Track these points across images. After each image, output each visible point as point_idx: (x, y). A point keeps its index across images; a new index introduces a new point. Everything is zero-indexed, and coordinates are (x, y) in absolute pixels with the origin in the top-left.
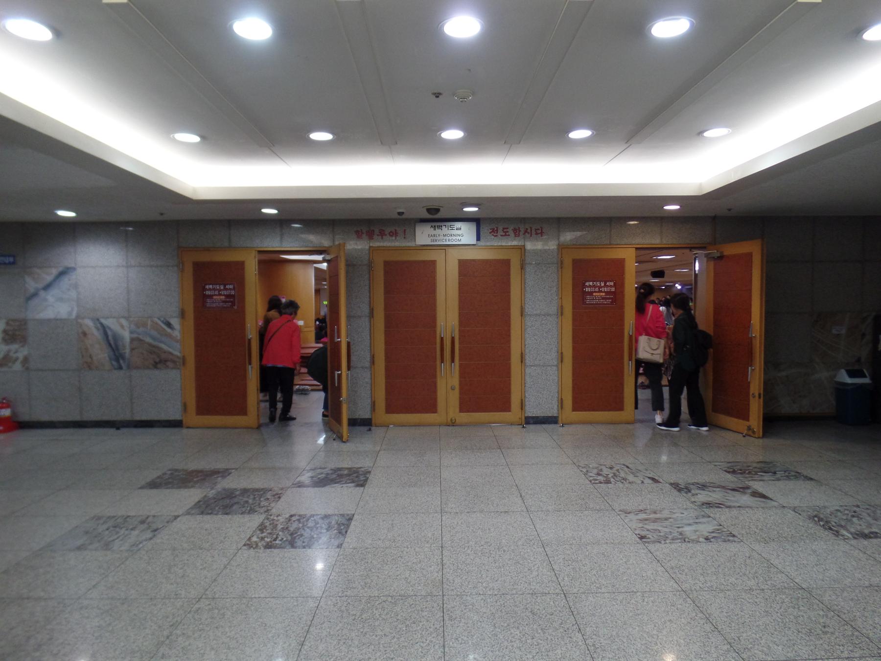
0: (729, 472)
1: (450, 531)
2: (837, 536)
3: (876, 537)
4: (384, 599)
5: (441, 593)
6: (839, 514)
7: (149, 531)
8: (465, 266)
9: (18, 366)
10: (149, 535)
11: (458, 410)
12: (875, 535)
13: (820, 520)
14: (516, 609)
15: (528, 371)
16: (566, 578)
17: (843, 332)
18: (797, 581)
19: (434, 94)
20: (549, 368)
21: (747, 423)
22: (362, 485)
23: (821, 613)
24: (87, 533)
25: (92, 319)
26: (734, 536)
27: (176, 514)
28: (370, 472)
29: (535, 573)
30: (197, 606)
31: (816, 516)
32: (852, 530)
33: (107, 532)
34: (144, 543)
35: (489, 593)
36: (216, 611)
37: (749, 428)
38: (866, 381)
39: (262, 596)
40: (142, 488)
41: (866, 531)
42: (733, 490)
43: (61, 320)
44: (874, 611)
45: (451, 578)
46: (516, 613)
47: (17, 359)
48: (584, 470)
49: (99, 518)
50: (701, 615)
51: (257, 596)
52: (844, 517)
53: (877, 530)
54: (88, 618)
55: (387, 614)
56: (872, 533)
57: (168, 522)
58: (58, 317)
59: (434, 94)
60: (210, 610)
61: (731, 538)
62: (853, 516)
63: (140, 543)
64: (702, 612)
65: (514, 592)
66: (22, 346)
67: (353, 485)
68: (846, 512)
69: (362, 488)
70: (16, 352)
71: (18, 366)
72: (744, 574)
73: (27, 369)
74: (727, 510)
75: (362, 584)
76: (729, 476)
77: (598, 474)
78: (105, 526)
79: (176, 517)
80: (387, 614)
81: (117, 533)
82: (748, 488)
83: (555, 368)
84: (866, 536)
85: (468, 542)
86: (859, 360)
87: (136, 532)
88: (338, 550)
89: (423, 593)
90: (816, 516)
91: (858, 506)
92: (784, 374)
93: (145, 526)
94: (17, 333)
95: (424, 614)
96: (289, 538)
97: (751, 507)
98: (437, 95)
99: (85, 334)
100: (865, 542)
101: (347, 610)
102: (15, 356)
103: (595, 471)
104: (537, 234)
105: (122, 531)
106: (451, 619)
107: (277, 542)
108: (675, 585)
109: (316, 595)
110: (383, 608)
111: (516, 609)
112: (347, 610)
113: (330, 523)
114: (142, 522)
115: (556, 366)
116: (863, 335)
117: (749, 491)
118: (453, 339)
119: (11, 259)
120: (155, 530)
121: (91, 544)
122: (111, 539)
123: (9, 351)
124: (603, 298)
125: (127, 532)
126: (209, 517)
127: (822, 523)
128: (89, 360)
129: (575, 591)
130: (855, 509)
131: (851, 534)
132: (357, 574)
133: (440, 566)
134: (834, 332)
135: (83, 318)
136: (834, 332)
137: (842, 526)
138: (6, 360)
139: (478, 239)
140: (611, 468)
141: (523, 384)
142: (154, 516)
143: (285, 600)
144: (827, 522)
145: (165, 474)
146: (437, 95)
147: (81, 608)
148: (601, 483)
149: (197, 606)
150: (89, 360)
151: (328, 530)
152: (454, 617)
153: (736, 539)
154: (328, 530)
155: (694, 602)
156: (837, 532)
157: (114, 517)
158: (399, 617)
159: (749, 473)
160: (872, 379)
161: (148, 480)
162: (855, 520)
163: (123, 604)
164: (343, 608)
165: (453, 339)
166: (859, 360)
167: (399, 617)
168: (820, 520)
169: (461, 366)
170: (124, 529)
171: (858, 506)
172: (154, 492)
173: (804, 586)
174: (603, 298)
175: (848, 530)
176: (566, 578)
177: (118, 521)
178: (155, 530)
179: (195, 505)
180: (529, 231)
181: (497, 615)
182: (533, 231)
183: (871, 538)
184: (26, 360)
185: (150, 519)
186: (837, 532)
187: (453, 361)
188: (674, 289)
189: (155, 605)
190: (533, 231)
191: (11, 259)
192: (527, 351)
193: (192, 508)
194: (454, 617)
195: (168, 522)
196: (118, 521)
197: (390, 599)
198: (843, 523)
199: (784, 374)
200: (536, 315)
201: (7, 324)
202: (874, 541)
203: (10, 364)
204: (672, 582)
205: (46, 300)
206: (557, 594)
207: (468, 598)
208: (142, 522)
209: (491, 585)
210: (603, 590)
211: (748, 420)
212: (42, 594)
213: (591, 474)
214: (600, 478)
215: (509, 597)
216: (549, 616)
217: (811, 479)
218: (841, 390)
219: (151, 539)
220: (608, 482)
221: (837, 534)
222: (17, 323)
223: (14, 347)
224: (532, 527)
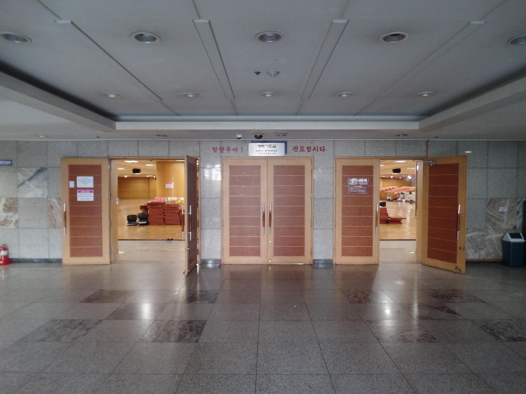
1: (263, 333)
2: (497, 339)
3: (521, 340)
4: (221, 376)
5: (255, 373)
9: (12, 226)
10: (84, 332)
12: (520, 339)
13: (488, 328)
14: (300, 384)
15: (315, 232)
16: (331, 364)
17: (506, 210)
18: (471, 368)
19: (256, 72)
20: (328, 230)
21: (454, 265)
23: (485, 389)
24: (47, 330)
26: (435, 339)
27: (101, 319)
29: (313, 361)
30: (109, 379)
31: (485, 326)
32: (507, 335)
33: (59, 330)
34: (81, 337)
35: (284, 373)
36: (120, 382)
37: (457, 268)
38: (522, 240)
39: (148, 373)
40: (81, 302)
41: (515, 337)
43: (38, 198)
44: (517, 389)
45: (262, 363)
46: (299, 387)
47: (11, 221)
48: (347, 294)
50: (411, 390)
51: (145, 373)
52: (503, 327)
53: (522, 336)
54: (43, 385)
55: (222, 386)
56: (519, 338)
57: (95, 324)
59: (256, 72)
60: (116, 381)
61: (433, 340)
62: (508, 326)
63: (78, 337)
64: (412, 388)
65: (299, 373)
66: (15, 214)
70: (11, 217)
71: (12, 226)
72: (439, 364)
75: (209, 366)
77: (355, 297)
78: (59, 326)
79: (101, 321)
80: (222, 386)
82: (445, 307)
83: (331, 230)
84: (515, 340)
85: (274, 340)
86: (515, 227)
87: (76, 330)
88: (195, 344)
89: (245, 373)
91: (511, 320)
92: (470, 235)
93: (81, 327)
94: (12, 206)
95: (245, 386)
96: (167, 336)
98: (258, 73)
99: (52, 207)
100: (515, 344)
101: (198, 383)
102: (10, 219)
104: (321, 150)
105: (68, 330)
106: (260, 390)
107: (160, 338)
108: (397, 370)
109: (181, 373)
110: (220, 382)
111: (300, 384)
112: (198, 383)
115: (333, 229)
116: (518, 212)
119: (9, 163)
120: (88, 329)
121: (48, 338)
122: (62, 334)
123: (7, 217)
125: (71, 330)
127: (488, 331)
128: (54, 222)
129: (336, 373)
130: (509, 321)
131: (506, 338)
132: (206, 360)
133: (256, 356)
134: (500, 210)
135: (51, 198)
136: (500, 210)
138: (5, 222)
139: (286, 152)
140: (363, 293)
141: (312, 240)
142: (88, 320)
143: (162, 376)
144: (492, 330)
146: (258, 73)
147: (40, 379)
148: (356, 302)
149: (109, 379)
151: (190, 331)
152: (262, 388)
153: (436, 341)
155: (407, 381)
156: (498, 336)
157: (64, 320)
158: (229, 388)
159: (447, 297)
162: (509, 329)
163: (65, 376)
164: (196, 382)
167: (229, 388)
168: (488, 328)
169: (275, 228)
170: (69, 328)
171: (511, 320)
172: (89, 304)
173: (475, 372)
175: (504, 336)
176: (331, 364)
177: (67, 322)
178: (88, 329)
179: (112, 313)
181: (288, 388)
183: (518, 341)
184: (17, 222)
185: (85, 322)
186: (498, 336)
187: (270, 225)
189: (84, 378)
191: (9, 163)
193: (110, 315)
194: (262, 388)
195: (95, 324)
196: (67, 322)
197: (224, 376)
199: (470, 235)
200: (320, 199)
201: (6, 200)
202: (520, 343)
203: (7, 224)
204: (396, 368)
206: (325, 375)
207: (271, 376)
209: (286, 368)
210: (353, 373)
211: (455, 262)
212: (18, 369)
213: (350, 297)
214: (355, 299)
215: (296, 376)
216: (319, 389)
217: (484, 302)
218: (506, 245)
219: (84, 335)
221: (497, 338)
222: (12, 200)
223: (10, 214)
224: (313, 331)
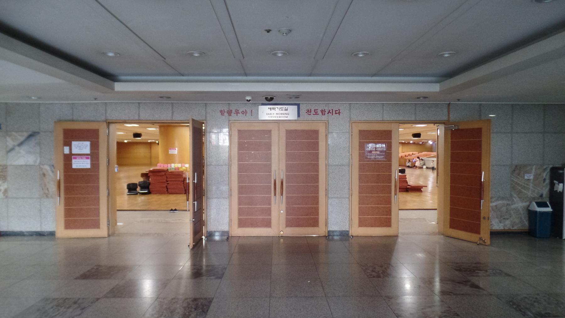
0: (457, 270)
1: (274, 311)
2: (524, 316)
6: (526, 300)
7: (79, 309)
8: (291, 134)
10: (78, 312)
11: (285, 226)
17: (532, 177)
20: (343, 200)
22: (220, 278)
25: (50, 166)
27: (98, 297)
28: (226, 269)
31: (511, 301)
33: (52, 310)
40: (76, 279)
41: (543, 312)
42: (459, 283)
48: (364, 268)
49: (47, 300)
53: (549, 311)
57: (92, 303)
58: (28, 164)
59: (266, 30)
62: (535, 302)
66: (4, 182)
67: (214, 277)
68: (531, 299)
69: (220, 280)
73: (7, 197)
74: (454, 297)
76: (457, 273)
77: (373, 271)
79: (98, 299)
81: (59, 310)
82: (469, 281)
87: (70, 310)
90: (511, 301)
91: (538, 294)
92: (494, 204)
97: (469, 295)
98: (268, 31)
103: (371, 269)
104: (336, 113)
113: (197, 304)
114: (75, 303)
116: (545, 180)
117: (469, 283)
118: (275, 194)
122: (54, 315)
124: (378, 155)
125: (65, 310)
126: (119, 299)
127: (515, 306)
128: (46, 192)
130: (536, 296)
134: (526, 178)
136: (526, 178)
137: (527, 308)
139: (299, 115)
140: (381, 266)
142: (83, 299)
145: (93, 269)
146: (268, 31)
148: (374, 277)
150: (46, 192)
151: (195, 309)
154: (195, 309)
156: (524, 313)
157: (57, 299)
160: (552, 208)
161: (81, 273)
165: (275, 194)
166: (541, 196)
168: (514, 304)
171: (538, 294)
174: (378, 155)
175: (531, 312)
177: (60, 301)
180: (331, 111)
182: (334, 112)
185: (80, 301)
187: (282, 194)
188: (428, 144)
190: (334, 112)
192: (329, 188)
195: (92, 303)
198: (528, 306)
199: (494, 204)
200: (335, 165)
205: (19, 152)
208: (75, 303)
213: (368, 271)
214: (374, 274)
219: (79, 315)
220: (379, 276)
224: (328, 308)
